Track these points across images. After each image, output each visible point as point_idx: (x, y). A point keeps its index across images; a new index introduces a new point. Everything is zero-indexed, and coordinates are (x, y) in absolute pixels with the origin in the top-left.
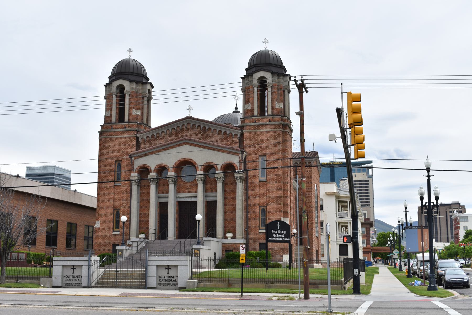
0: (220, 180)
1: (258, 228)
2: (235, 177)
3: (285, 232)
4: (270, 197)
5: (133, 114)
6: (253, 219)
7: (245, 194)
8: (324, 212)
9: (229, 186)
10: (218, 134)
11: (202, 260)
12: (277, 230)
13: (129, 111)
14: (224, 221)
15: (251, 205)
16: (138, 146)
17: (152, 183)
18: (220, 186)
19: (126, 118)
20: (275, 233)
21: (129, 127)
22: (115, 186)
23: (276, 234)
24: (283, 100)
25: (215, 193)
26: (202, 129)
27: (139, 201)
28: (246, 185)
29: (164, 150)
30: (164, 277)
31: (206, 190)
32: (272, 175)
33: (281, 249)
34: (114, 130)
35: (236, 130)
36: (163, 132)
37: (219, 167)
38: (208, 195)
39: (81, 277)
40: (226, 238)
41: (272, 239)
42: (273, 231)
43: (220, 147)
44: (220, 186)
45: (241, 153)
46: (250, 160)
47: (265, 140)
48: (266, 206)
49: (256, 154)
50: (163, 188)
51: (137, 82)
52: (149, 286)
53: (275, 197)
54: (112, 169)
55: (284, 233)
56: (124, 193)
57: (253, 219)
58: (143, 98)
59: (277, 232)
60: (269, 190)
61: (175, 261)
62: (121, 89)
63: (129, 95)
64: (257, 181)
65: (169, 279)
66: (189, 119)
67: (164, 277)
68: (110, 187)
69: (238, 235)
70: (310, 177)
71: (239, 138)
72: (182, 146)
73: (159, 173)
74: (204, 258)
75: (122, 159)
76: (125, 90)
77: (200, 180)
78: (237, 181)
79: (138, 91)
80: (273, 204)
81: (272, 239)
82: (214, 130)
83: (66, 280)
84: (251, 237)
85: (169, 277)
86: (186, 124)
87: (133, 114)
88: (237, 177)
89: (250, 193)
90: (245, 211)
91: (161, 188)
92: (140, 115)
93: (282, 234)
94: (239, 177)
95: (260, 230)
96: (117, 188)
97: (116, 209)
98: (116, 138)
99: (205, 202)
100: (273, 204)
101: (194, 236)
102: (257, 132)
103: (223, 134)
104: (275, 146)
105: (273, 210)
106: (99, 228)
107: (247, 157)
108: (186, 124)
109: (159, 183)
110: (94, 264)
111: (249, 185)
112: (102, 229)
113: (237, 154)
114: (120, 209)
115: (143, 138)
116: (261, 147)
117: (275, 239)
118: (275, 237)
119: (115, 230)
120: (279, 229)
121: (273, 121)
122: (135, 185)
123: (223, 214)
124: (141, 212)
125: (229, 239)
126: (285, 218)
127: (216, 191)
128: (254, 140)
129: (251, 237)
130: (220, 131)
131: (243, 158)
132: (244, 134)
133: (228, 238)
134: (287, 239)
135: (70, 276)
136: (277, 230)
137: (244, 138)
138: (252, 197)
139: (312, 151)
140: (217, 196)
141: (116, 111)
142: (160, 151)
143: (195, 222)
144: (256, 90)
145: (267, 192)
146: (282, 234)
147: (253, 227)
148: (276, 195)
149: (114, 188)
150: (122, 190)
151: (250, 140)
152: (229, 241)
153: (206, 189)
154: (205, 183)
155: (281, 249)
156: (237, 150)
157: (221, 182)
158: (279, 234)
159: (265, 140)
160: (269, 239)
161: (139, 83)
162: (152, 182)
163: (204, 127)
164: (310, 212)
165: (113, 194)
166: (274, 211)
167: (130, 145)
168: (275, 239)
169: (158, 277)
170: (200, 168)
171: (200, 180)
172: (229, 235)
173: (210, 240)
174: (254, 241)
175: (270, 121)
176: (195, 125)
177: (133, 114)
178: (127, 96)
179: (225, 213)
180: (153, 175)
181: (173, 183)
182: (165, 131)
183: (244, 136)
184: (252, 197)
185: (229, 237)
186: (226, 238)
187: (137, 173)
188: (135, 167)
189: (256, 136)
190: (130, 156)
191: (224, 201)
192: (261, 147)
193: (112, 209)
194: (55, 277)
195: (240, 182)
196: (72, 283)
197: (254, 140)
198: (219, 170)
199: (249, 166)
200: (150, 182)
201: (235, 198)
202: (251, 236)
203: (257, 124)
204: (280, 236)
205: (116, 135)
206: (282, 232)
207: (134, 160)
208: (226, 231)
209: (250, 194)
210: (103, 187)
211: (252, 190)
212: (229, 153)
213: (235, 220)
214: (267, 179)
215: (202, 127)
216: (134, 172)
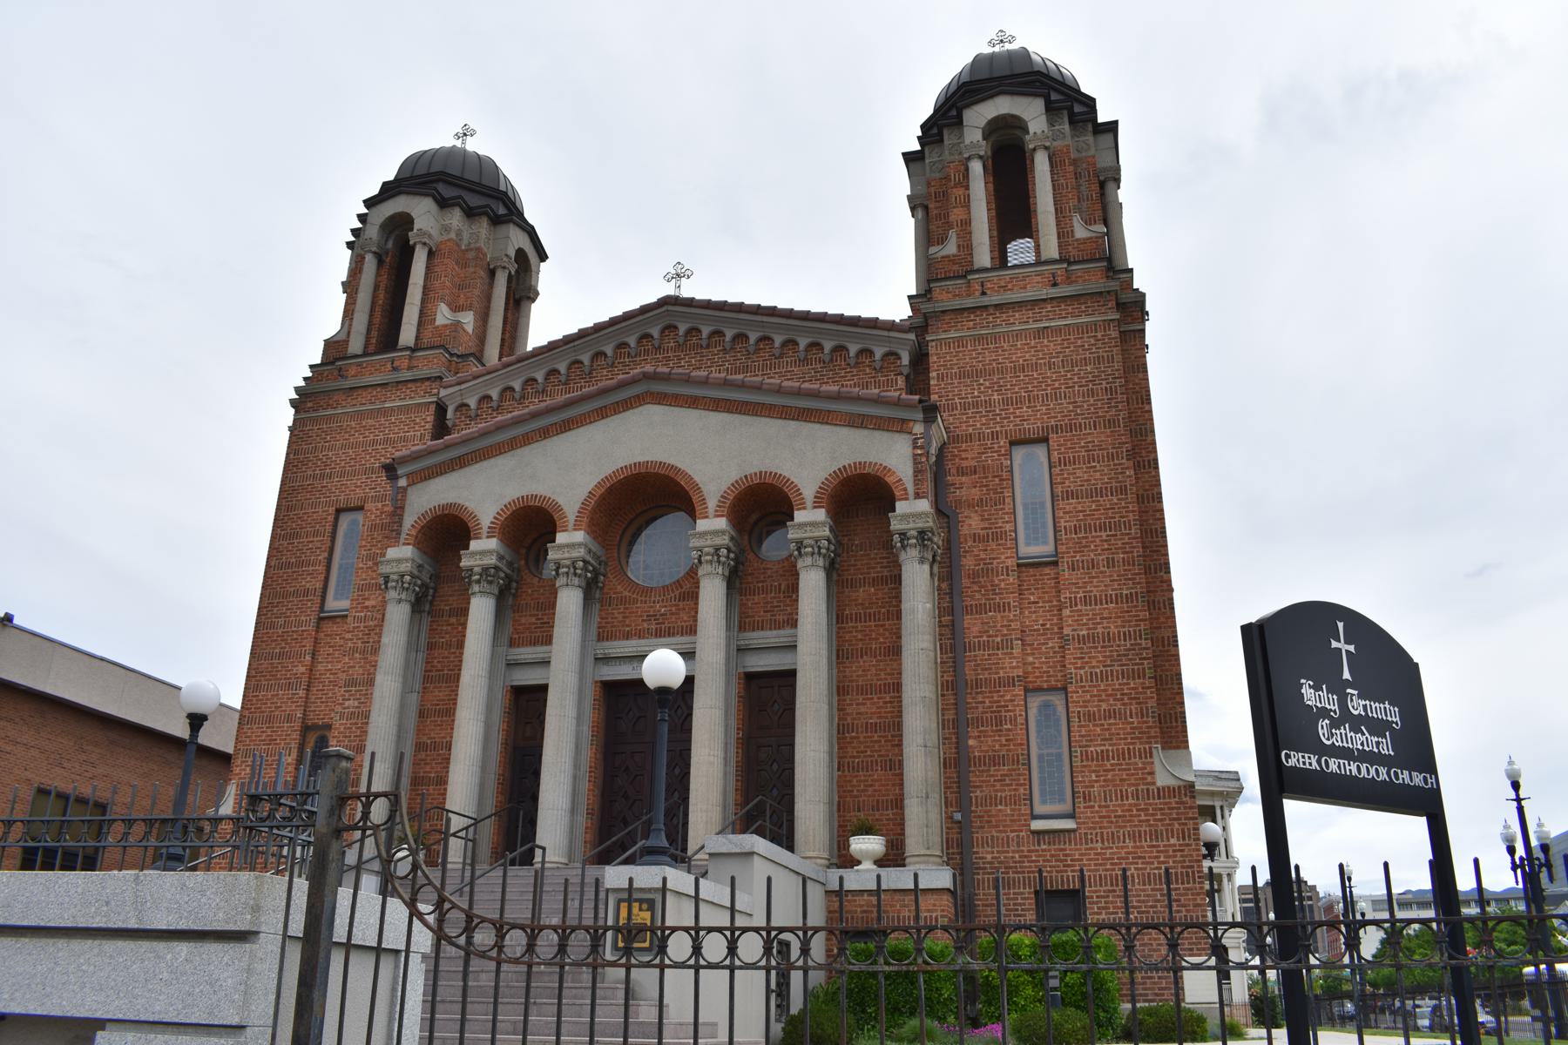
0: (816, 556)
1: (1025, 810)
5: (437, 323)
6: (995, 761)
7: (947, 631)
9: (861, 594)
10: (806, 358)
13: (422, 313)
14: (836, 773)
15: (978, 683)
16: (441, 428)
17: (476, 588)
18: (812, 584)
19: (407, 335)
20: (1324, 713)
21: (410, 368)
23: (1335, 724)
24: (1099, 213)
25: (788, 631)
26: (728, 346)
27: (418, 686)
28: (951, 586)
29: (545, 433)
31: (741, 619)
32: (1088, 528)
34: (348, 383)
35: (893, 334)
36: (555, 372)
37: (809, 491)
38: (754, 643)
40: (847, 861)
43: (815, 395)
44: (812, 584)
45: (920, 416)
46: (965, 464)
48: (1065, 689)
49: (995, 436)
50: (533, 620)
51: (471, 209)
54: (319, 545)
55: (1387, 725)
56: (354, 650)
57: (995, 761)
58: (492, 273)
59: (1343, 704)
60: (1073, 602)
61: (62, 946)
62: (401, 224)
63: (431, 254)
64: (1009, 562)
66: (670, 308)
68: (300, 624)
69: (914, 842)
71: (906, 371)
72: (629, 413)
73: (523, 551)
75: (365, 500)
76: (412, 230)
77: (711, 562)
78: (903, 556)
79: (470, 243)
80: (1104, 677)
82: (785, 344)
84: (989, 857)
86: (655, 332)
87: (437, 323)
88: (903, 535)
89: (972, 625)
90: (950, 715)
91: (523, 620)
92: (470, 329)
94: (914, 533)
95: (1035, 817)
96: (328, 627)
97: (315, 727)
98: (352, 416)
99: (734, 681)
100: (1104, 677)
102: (996, 337)
103: (827, 359)
104: (1092, 393)
105: (1104, 706)
107: (953, 449)
108: (655, 332)
109: (515, 596)
111: (965, 582)
113: (899, 426)
114: (329, 727)
115: (463, 406)
116: (1020, 401)
117: (1333, 765)
121: (1069, 280)
122: (400, 601)
123: (831, 736)
124: (424, 739)
125: (867, 865)
126: (1172, 752)
127: (793, 623)
128: (979, 374)
129: (989, 857)
130: (816, 345)
131: (933, 450)
132: (932, 351)
133: (859, 863)
136: (1338, 688)
137: (933, 366)
138: (985, 646)
140: (799, 644)
141: (371, 316)
142: (526, 440)
144: (976, 167)
145: (1066, 612)
147: (995, 801)
148: (1113, 629)
149: (318, 628)
150: (349, 636)
151: (962, 375)
152: (862, 878)
153: (743, 616)
154: (736, 581)
156: (897, 403)
157: (821, 562)
158: (1357, 723)
160: (1292, 762)
161: (480, 214)
162: (478, 582)
163: (741, 337)
165: (308, 658)
166: (1109, 714)
170: (712, 504)
171: (711, 562)
172: (867, 845)
173: (752, 854)
175: (1055, 285)
176: (700, 331)
177: (440, 321)
179: (843, 733)
180: (484, 549)
181: (576, 581)
182: (562, 368)
184: (985, 646)
185: (867, 854)
186: (848, 861)
187: (414, 545)
188: (410, 520)
189: (988, 357)
191: (835, 671)
192: (1020, 401)
193: (297, 725)
195: (922, 561)
198: (809, 504)
199: (962, 493)
200: (470, 583)
201: (895, 651)
202: (987, 854)
203: (995, 299)
204: (1362, 741)
205: (354, 402)
207: (405, 489)
208: (845, 825)
209: (975, 629)
211: (981, 609)
212: (862, 426)
213: (895, 766)
214: (1062, 549)
215: (728, 338)
216: (402, 540)
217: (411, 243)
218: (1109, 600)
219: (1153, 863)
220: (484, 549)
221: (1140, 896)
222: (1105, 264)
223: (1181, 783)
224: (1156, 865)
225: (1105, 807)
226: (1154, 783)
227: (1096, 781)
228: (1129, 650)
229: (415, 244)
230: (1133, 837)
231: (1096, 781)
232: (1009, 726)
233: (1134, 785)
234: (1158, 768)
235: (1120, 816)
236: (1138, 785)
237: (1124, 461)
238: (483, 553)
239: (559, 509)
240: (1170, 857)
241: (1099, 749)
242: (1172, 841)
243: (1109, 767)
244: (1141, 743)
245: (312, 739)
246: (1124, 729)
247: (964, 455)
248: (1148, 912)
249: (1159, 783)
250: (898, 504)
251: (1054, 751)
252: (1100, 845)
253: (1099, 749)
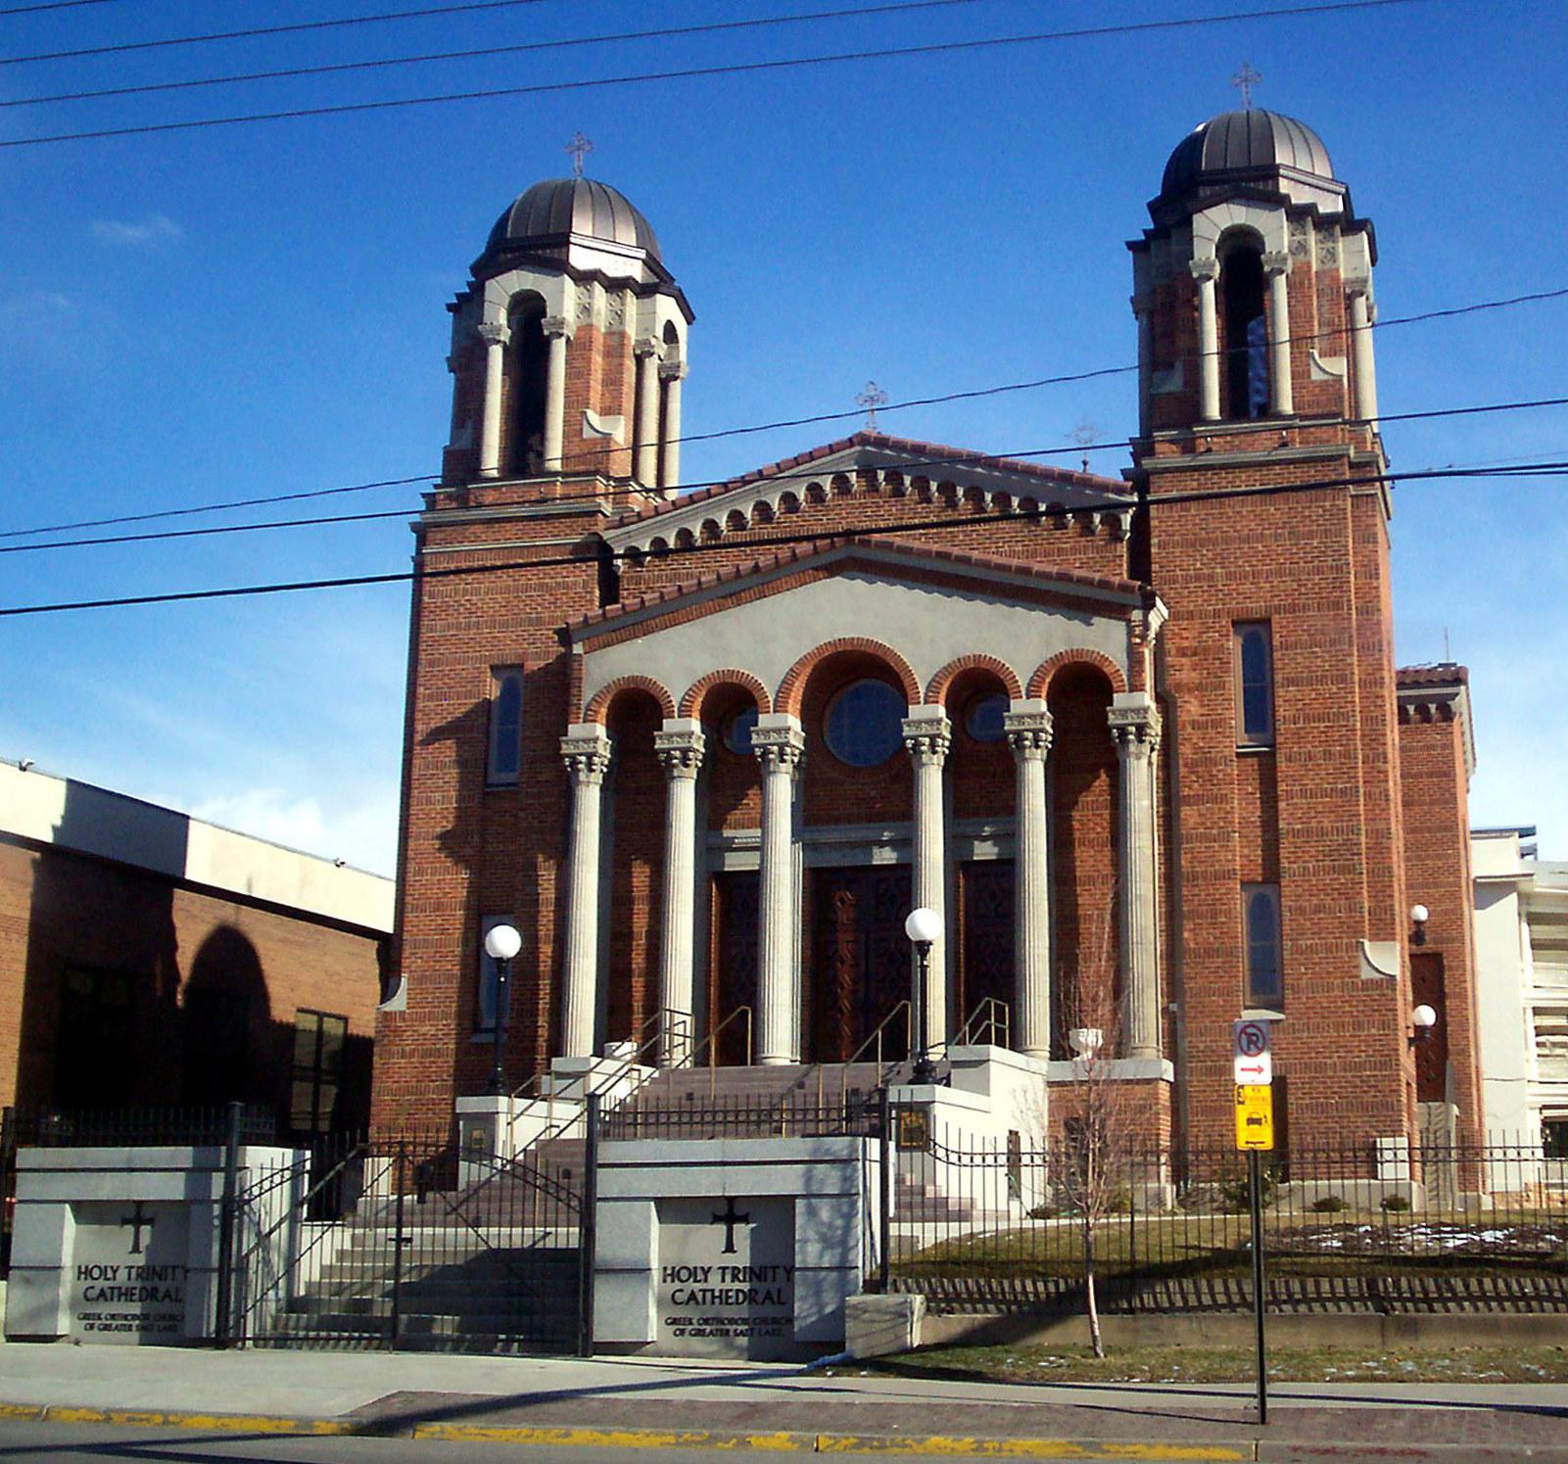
2: (1109, 729)
4: (1295, 833)
11: (953, 1158)
22: (487, 794)
30: (110, 1274)
32: (1307, 719)
39: (179, 1273)
52: (601, 1334)
53: (1322, 832)
65: (737, 1285)
67: (110, 1274)
70: (1446, 774)
74: (978, 1149)
83: (90, 1293)
85: (735, 1278)
89: (1188, 815)
101: (896, 1049)
104: (1319, 571)
106: (402, 1013)
110: (266, 1185)
111: (1183, 771)
112: (422, 1019)
131: (1152, 634)
135: (115, 1272)
139: (1440, 665)
143: (911, 952)
147: (1209, 992)
148: (1326, 824)
150: (522, 814)
164: (1453, 940)
165: (476, 838)
166: (1318, 910)
167: (566, 586)
169: (80, 1273)
183: (1154, 523)
190: (565, 636)
194: (26, 1273)
196: (125, 1317)
210: (429, 801)
211: (1199, 799)
242: (1373, 1031)
249: (1364, 977)
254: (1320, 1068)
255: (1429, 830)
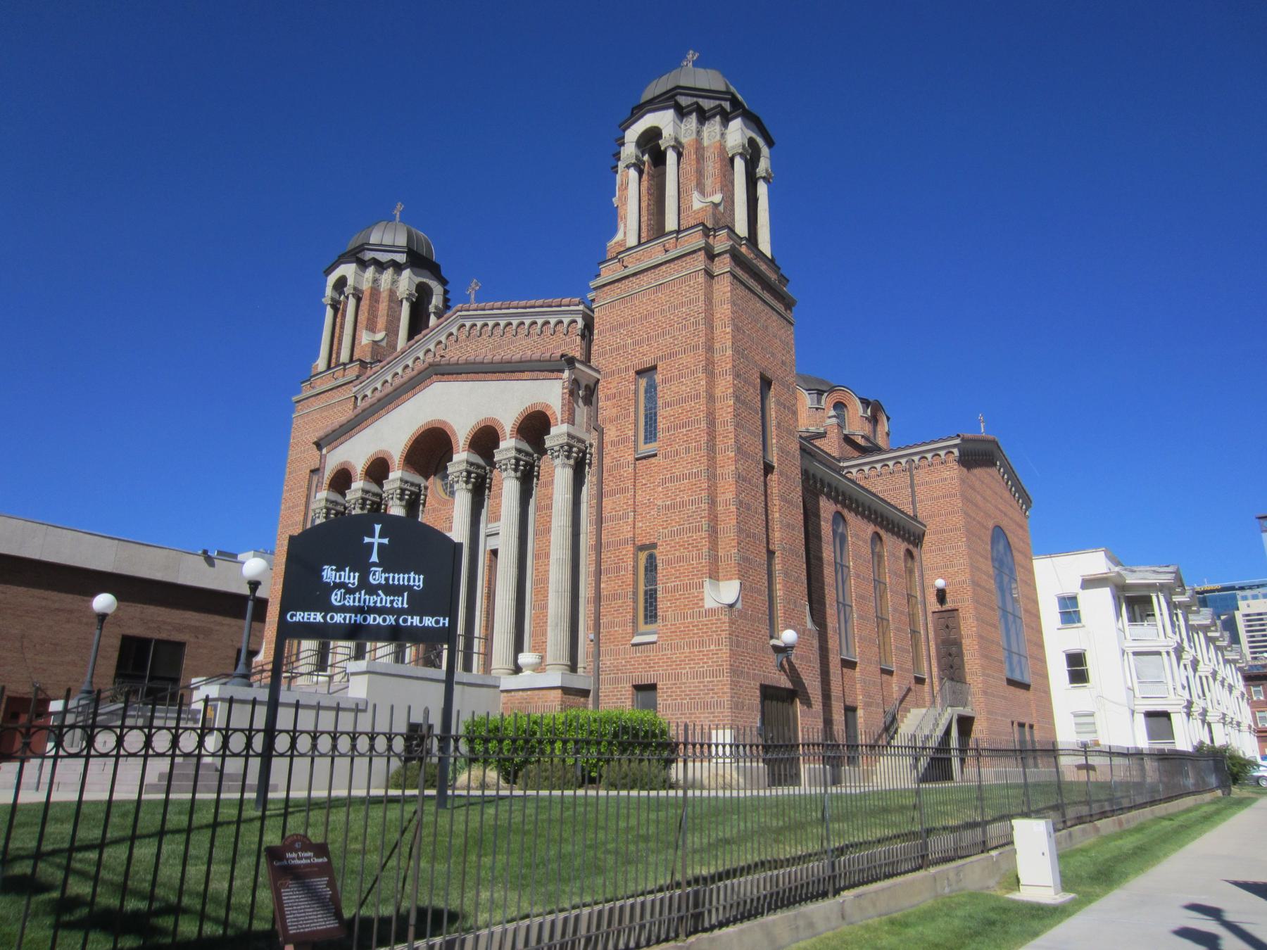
3: (417, 581)
4: (667, 508)
8: (1084, 626)
12: (363, 568)
19: (671, 224)
23: (350, 591)
33: (706, 705)
41: (318, 617)
42: (329, 574)
47: (652, 314)
53: (683, 504)
55: (409, 588)
80: (679, 533)
81: (318, 617)
87: (363, 343)
93: (391, 590)
100: (679, 533)
105: (677, 554)
118: (343, 609)
119: (642, 627)
120: (374, 564)
128: (621, 325)
129: (608, 663)
134: (429, 621)
136: (363, 568)
146: (391, 590)
148: (686, 498)
151: (613, 328)
155: (706, 705)
158: (372, 590)
159: (652, 314)
166: (680, 559)
168: (338, 618)
174: (617, 681)
178: (671, 157)
186: (517, 670)
195: (564, 465)
197: (621, 325)
204: (382, 600)
206: (399, 579)
217: (662, 148)
218: (684, 477)
219: (699, 663)
220: (508, 446)
221: (690, 687)
222: (701, 228)
223: (720, 605)
224: (701, 665)
225: (674, 625)
226: (703, 607)
227: (670, 607)
228: (694, 512)
229: (666, 149)
230: (689, 645)
231: (670, 607)
232: (623, 573)
233: (691, 608)
234: (706, 596)
235: (682, 631)
236: (693, 608)
237: (700, 374)
238: (507, 450)
239: (354, 468)
240: (710, 658)
241: (672, 585)
242: (712, 647)
243: (678, 597)
244: (697, 578)
245: (643, 556)
246: (688, 569)
247: (609, 386)
248: (695, 698)
249: (707, 606)
250: (552, 429)
251: (653, 587)
252: (669, 652)
253: (672, 585)
254: (677, 676)
255: (945, 531)
